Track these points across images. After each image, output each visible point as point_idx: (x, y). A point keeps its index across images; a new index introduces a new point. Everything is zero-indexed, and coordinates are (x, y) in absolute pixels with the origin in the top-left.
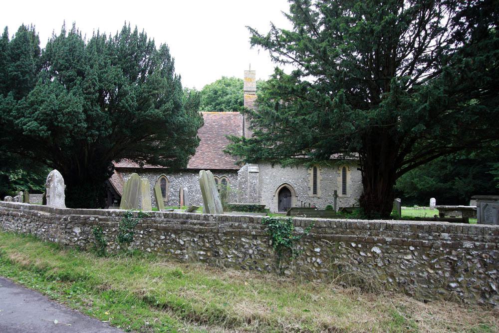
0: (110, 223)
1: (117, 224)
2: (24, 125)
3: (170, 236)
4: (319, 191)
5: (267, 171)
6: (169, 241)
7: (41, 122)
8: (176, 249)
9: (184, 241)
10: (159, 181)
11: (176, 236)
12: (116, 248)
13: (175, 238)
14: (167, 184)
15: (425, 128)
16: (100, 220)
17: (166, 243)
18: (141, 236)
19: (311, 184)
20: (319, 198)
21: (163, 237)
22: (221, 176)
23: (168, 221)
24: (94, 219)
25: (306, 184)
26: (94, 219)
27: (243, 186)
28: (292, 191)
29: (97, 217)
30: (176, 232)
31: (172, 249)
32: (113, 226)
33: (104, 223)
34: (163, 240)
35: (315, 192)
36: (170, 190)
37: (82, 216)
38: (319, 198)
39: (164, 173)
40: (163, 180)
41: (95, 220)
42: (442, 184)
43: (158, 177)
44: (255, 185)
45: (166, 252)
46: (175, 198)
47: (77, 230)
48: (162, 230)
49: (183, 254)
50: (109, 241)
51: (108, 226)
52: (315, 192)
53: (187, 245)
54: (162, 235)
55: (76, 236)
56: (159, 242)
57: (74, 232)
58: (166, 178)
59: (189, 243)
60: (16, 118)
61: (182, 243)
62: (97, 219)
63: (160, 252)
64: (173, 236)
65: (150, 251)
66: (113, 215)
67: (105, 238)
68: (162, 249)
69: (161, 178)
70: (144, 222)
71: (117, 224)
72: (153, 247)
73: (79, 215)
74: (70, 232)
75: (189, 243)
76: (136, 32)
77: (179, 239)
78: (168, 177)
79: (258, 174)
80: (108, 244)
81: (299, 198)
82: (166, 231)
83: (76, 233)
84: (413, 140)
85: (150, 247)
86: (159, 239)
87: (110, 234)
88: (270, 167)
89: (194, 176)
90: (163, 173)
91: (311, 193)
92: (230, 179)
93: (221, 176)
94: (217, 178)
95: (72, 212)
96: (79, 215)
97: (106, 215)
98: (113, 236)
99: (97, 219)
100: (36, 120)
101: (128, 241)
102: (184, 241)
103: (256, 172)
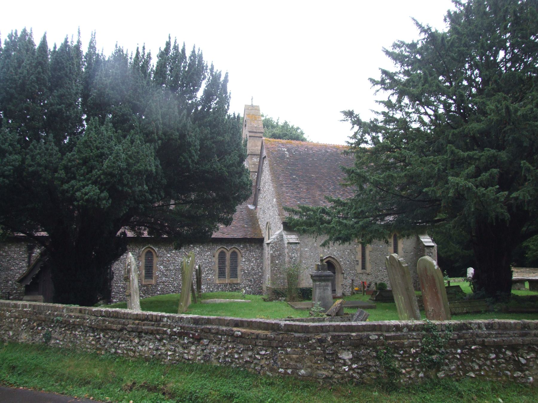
0: (406, 342)
1: (418, 342)
2: (78, 190)
3: (504, 353)
4: (368, 265)
5: (306, 241)
6: (503, 360)
7: (102, 185)
8: (513, 371)
9: (527, 359)
10: (143, 257)
11: (512, 352)
12: (417, 376)
13: (513, 355)
14: (155, 260)
15: (449, 195)
16: (387, 338)
17: (499, 363)
18: (458, 356)
19: (359, 257)
20: (368, 274)
21: (493, 356)
22: (230, 248)
23: (499, 334)
24: (377, 337)
25: (353, 257)
26: (377, 337)
27: (277, 262)
28: (337, 267)
29: (382, 335)
30: (513, 348)
31: (508, 370)
32: (411, 346)
33: (397, 343)
34: (493, 359)
35: (364, 267)
36: (159, 268)
37: (354, 334)
38: (368, 274)
39: (151, 243)
40: (149, 255)
41: (379, 339)
42: (466, 251)
43: (143, 250)
44: (295, 260)
45: (497, 375)
46: (167, 279)
47: (347, 356)
48: (492, 346)
49: (526, 377)
50: (404, 368)
51: (402, 346)
52: (364, 267)
53: (531, 364)
54: (492, 353)
55: (345, 364)
56: (488, 363)
57: (340, 358)
58: (152, 251)
59: (533, 361)
60: (63, 181)
61: (523, 361)
62: (381, 337)
63: (489, 376)
64: (509, 353)
65: (473, 376)
66: (405, 330)
67: (396, 364)
68: (493, 372)
69: (146, 251)
70: (460, 337)
71: (418, 342)
72: (477, 370)
73: (347, 334)
74: (334, 359)
75: (533, 361)
76: (44, 43)
77: (517, 356)
78: (156, 249)
79: (299, 246)
80: (404, 371)
81: (345, 275)
82: (498, 348)
83: (344, 360)
84: (385, 200)
85: (473, 370)
86: (486, 359)
87: (405, 357)
88: (414, 246)
89: (193, 247)
90: (148, 244)
91: (359, 268)
92: (242, 251)
93: (230, 248)
94: (225, 250)
95: (331, 329)
96: (347, 334)
97: (393, 331)
98: (411, 360)
99: (381, 337)
100: (95, 183)
101: (436, 366)
102: (527, 359)
103: (296, 243)
